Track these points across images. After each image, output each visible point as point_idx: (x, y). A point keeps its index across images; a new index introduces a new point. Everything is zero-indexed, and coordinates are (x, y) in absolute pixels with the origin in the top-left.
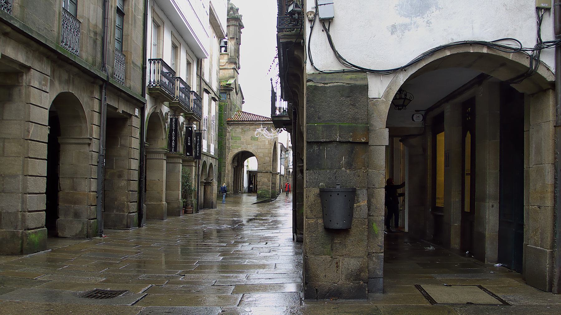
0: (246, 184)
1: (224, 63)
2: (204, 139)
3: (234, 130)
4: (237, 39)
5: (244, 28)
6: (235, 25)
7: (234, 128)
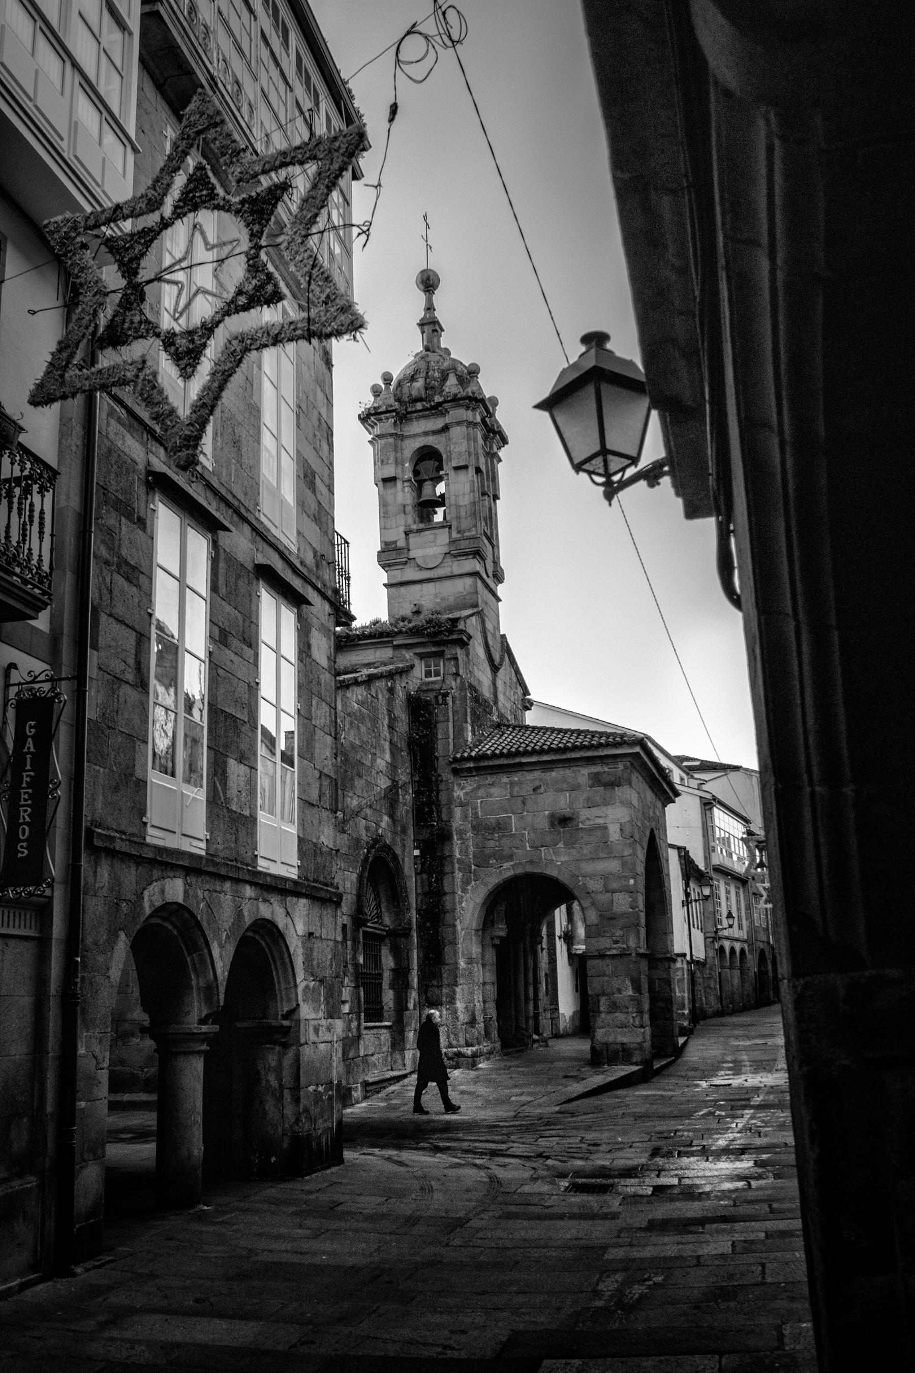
0: (567, 1005)
1: (435, 556)
2: (262, 808)
3: (481, 792)
4: (478, 470)
5: (507, 443)
6: (471, 424)
7: (479, 787)
